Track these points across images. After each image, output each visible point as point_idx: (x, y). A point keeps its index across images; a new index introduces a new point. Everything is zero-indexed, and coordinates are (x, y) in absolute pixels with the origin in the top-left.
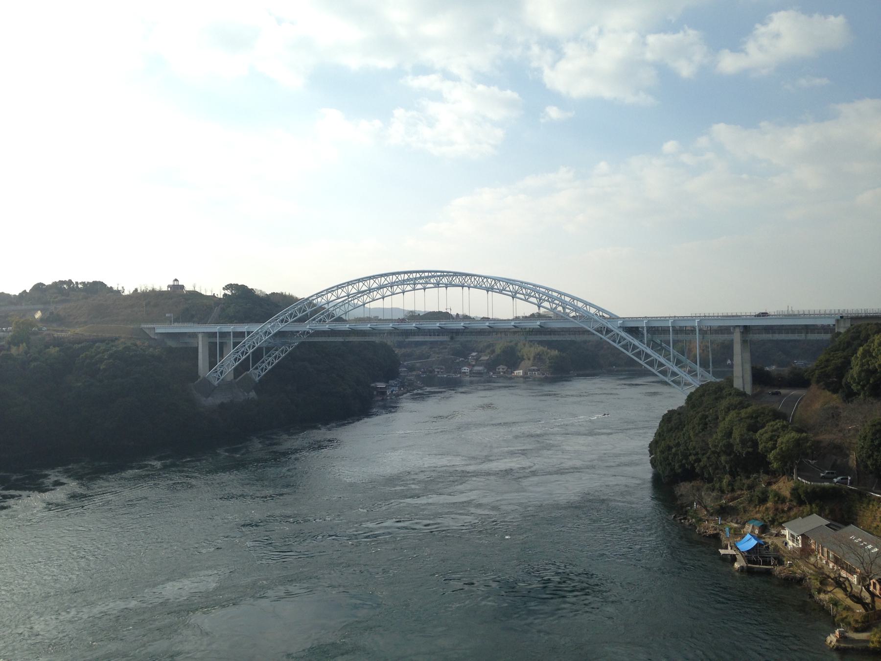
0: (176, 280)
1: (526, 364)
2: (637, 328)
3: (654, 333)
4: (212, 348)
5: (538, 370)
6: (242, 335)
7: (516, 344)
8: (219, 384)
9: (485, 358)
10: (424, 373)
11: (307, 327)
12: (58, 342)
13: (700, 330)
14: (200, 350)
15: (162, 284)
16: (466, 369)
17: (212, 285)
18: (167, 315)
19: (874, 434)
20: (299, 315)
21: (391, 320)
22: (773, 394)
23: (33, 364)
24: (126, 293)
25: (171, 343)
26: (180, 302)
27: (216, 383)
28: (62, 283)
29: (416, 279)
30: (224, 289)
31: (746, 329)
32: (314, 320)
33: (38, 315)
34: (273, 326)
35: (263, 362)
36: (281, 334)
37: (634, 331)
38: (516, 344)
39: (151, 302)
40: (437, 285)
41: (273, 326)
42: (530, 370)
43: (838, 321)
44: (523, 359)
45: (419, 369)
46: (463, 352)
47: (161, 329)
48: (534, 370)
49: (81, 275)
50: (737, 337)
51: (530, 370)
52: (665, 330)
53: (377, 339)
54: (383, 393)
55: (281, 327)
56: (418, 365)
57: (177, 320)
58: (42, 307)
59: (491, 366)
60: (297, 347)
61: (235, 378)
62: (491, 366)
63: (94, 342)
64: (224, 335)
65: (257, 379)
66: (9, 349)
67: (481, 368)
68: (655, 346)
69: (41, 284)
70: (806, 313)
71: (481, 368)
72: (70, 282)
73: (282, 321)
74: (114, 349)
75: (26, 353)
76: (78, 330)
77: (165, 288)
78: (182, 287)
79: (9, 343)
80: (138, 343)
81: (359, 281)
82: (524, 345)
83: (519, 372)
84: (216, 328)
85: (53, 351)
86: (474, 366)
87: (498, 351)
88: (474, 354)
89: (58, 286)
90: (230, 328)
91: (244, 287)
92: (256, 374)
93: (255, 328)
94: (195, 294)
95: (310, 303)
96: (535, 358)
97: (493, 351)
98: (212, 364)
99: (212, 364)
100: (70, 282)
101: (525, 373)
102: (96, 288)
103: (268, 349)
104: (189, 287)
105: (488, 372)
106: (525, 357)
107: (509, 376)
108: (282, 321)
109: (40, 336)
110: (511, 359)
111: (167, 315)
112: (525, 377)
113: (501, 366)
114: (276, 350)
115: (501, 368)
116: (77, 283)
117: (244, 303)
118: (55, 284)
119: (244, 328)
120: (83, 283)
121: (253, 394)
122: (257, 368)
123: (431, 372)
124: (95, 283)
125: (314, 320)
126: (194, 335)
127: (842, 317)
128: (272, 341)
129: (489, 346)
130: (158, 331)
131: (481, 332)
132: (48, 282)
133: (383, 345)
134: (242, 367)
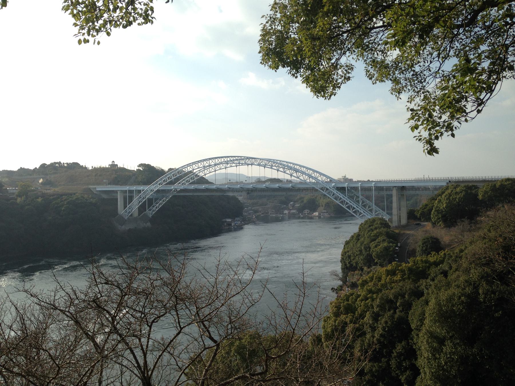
0: (113, 162)
1: (321, 209)
2: (356, 187)
3: (347, 189)
4: (125, 199)
5: (327, 212)
6: (139, 191)
7: (316, 197)
8: (128, 218)
9: (297, 205)
10: (262, 214)
11: (178, 186)
12: (43, 195)
13: (348, 189)
14: (119, 200)
15: (105, 164)
16: (286, 212)
17: (132, 165)
18: (104, 181)
19: (423, 244)
20: (191, 181)
21: (252, 183)
22: (416, 224)
23: (27, 207)
24: (38, 168)
25: (105, 196)
26: (116, 174)
27: (126, 218)
28: (55, 163)
29: (234, 160)
30: (138, 166)
31: (403, 188)
32: (179, 183)
33: (41, 181)
34: (155, 187)
35: (153, 207)
36: (158, 191)
37: (342, 189)
38: (316, 197)
39: (99, 172)
40: (259, 165)
41: (155, 187)
42: (322, 212)
43: (447, 183)
44: (320, 206)
45: (260, 212)
46: (285, 202)
47: (100, 188)
48: (324, 212)
49: (66, 159)
50: (394, 192)
51: (322, 212)
52: (369, 189)
53: (231, 194)
54: (229, 224)
55: (159, 187)
56: (260, 209)
57: (110, 184)
58: (43, 176)
59: (301, 210)
60: (171, 198)
61: (139, 215)
62: (301, 210)
63: (62, 195)
64: (131, 192)
65: (151, 216)
66: (16, 200)
67: (294, 211)
68: (351, 198)
69: (45, 164)
70: (434, 179)
71: (294, 211)
72: (60, 163)
73: (159, 184)
74: (71, 199)
75: (24, 201)
76: (56, 189)
77: (107, 166)
78: (117, 165)
79: (17, 196)
80: (86, 196)
81: (204, 160)
82: (321, 198)
83: (316, 214)
84: (127, 188)
85: (40, 200)
86: (291, 210)
87: (305, 201)
88: (292, 203)
89: (53, 165)
90: (134, 188)
91: (148, 166)
92: (150, 213)
93: (146, 188)
94: (123, 170)
95: (196, 175)
96: (325, 205)
97: (303, 201)
98: (125, 207)
99: (125, 207)
100: (60, 163)
101: (320, 214)
102: (75, 165)
103: (156, 199)
104: (120, 165)
105: (299, 214)
106: (320, 205)
107: (310, 216)
108: (159, 184)
109: (35, 192)
110: (312, 205)
111: (104, 181)
112: (319, 217)
113: (306, 210)
114: (160, 200)
115: (306, 211)
116: (64, 163)
117: (149, 173)
118: (52, 164)
119: (141, 188)
120: (67, 163)
121: (149, 224)
122: (150, 210)
123: (267, 213)
124: (74, 163)
125: (179, 183)
126: (116, 192)
127: (450, 181)
128: (155, 195)
129: (301, 198)
130: (97, 189)
131: (299, 190)
132: (48, 163)
133: (234, 198)
134: (142, 208)
